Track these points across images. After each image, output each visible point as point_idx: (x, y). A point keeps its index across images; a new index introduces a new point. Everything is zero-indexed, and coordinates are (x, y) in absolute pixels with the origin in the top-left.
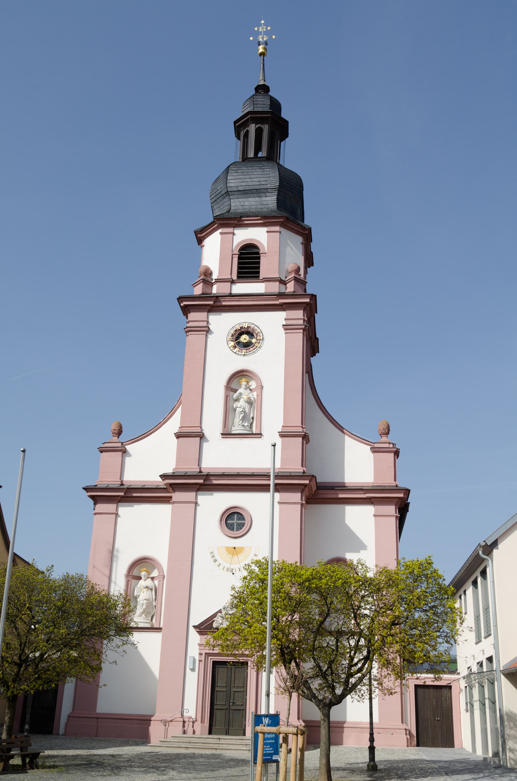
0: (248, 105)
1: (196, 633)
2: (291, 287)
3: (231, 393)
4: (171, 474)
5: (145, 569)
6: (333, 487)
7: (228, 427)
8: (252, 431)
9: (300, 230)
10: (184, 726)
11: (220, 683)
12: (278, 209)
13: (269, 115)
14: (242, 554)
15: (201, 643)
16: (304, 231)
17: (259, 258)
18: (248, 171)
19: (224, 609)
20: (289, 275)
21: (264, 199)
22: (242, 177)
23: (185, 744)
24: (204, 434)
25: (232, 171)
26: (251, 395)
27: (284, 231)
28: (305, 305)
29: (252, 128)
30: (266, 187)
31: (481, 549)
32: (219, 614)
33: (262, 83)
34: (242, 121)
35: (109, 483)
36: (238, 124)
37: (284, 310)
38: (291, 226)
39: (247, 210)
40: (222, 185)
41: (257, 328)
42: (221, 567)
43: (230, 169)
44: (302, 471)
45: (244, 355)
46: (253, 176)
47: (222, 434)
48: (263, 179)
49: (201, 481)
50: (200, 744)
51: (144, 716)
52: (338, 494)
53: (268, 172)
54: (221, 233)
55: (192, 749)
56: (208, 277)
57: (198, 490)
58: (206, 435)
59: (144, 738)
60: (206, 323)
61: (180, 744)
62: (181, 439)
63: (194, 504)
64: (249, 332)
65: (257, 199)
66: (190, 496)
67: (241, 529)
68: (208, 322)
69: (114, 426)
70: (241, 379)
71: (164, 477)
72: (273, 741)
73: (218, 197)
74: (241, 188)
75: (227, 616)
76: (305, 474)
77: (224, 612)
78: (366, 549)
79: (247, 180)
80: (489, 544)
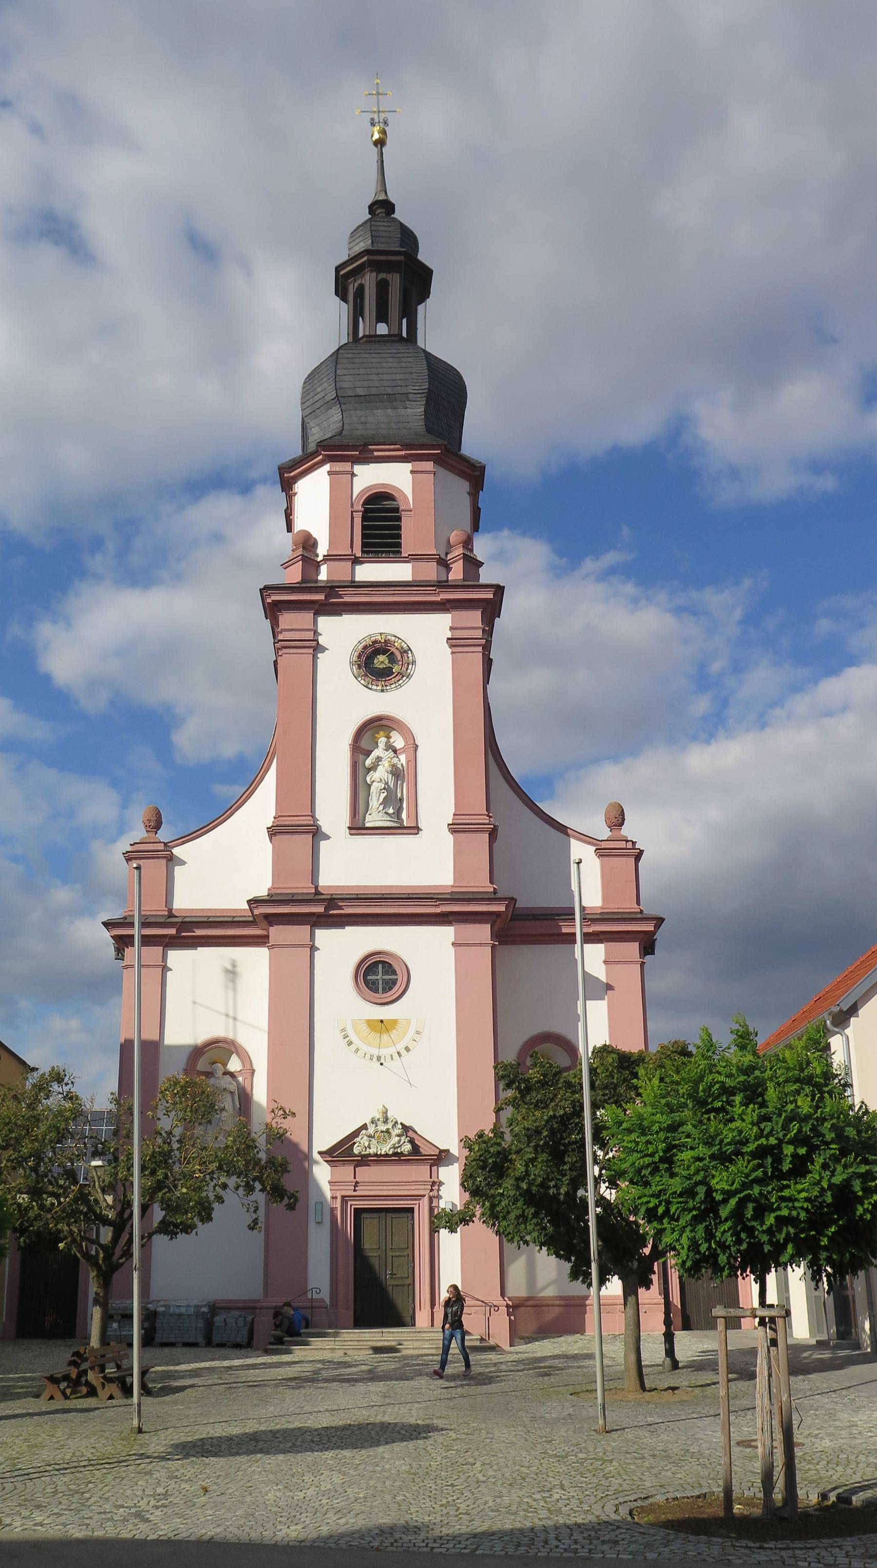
3: (361, 757)
4: (266, 898)
6: (534, 915)
9: (466, 469)
12: (429, 430)
13: (401, 258)
14: (394, 1031)
17: (399, 519)
18: (372, 360)
21: (402, 411)
22: (362, 371)
29: (369, 280)
30: (404, 390)
32: (364, 1132)
40: (326, 385)
43: (340, 356)
44: (492, 890)
45: (382, 691)
46: (382, 371)
47: (349, 828)
48: (398, 377)
50: (352, 1343)
54: (329, 473)
62: (279, 837)
63: (309, 949)
66: (301, 932)
67: (391, 989)
70: (378, 733)
71: (254, 902)
73: (318, 405)
74: (360, 392)
77: (371, 1130)
79: (371, 377)
80: (845, 1010)
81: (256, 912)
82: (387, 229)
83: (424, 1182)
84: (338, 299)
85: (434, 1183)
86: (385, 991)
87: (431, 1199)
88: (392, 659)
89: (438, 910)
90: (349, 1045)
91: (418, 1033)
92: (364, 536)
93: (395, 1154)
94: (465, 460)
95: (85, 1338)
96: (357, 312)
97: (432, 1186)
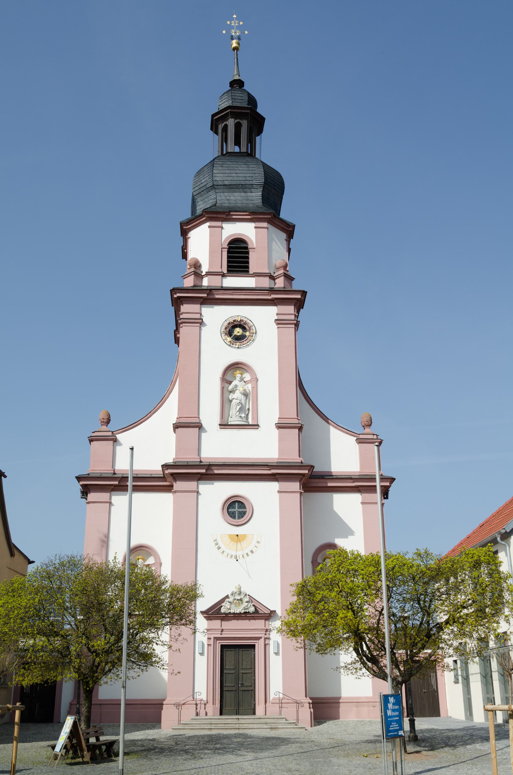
0: (226, 100)
1: (204, 618)
2: (280, 283)
3: (227, 385)
4: (172, 464)
5: (140, 557)
6: (322, 476)
8: (248, 422)
10: (197, 709)
11: (228, 665)
13: (249, 111)
14: (245, 542)
15: (209, 628)
16: (288, 228)
17: (248, 253)
18: (233, 166)
19: (232, 594)
20: (277, 271)
21: (249, 194)
22: (228, 171)
23: (207, 725)
25: (218, 165)
26: (245, 387)
27: (272, 228)
28: (296, 301)
29: (231, 123)
30: (251, 182)
31: (499, 536)
32: (227, 600)
33: (237, 78)
34: (220, 115)
35: (102, 472)
36: (216, 117)
38: (277, 222)
39: (233, 205)
40: (207, 178)
42: (225, 554)
43: (215, 163)
47: (220, 425)
48: (248, 175)
49: (204, 471)
50: (221, 725)
51: (147, 700)
52: (327, 483)
53: (254, 169)
54: (209, 227)
55: (215, 730)
56: (197, 269)
57: (199, 479)
58: (204, 425)
59: (155, 721)
61: (202, 725)
64: (241, 325)
65: (243, 194)
66: (191, 485)
67: (242, 517)
69: (102, 415)
70: (236, 371)
71: (165, 466)
72: (398, 718)
74: (226, 183)
75: (235, 601)
76: (303, 464)
78: (354, 535)
79: (232, 175)
80: (508, 531)
81: (167, 472)
82: (240, 95)
83: (261, 630)
84: (212, 132)
85: (267, 631)
86: (239, 518)
87: (265, 639)
88: (244, 329)
89: (270, 472)
90: (218, 549)
91: (258, 542)
92: (228, 262)
93: (245, 613)
94: (282, 221)
96: (225, 139)
97: (266, 632)
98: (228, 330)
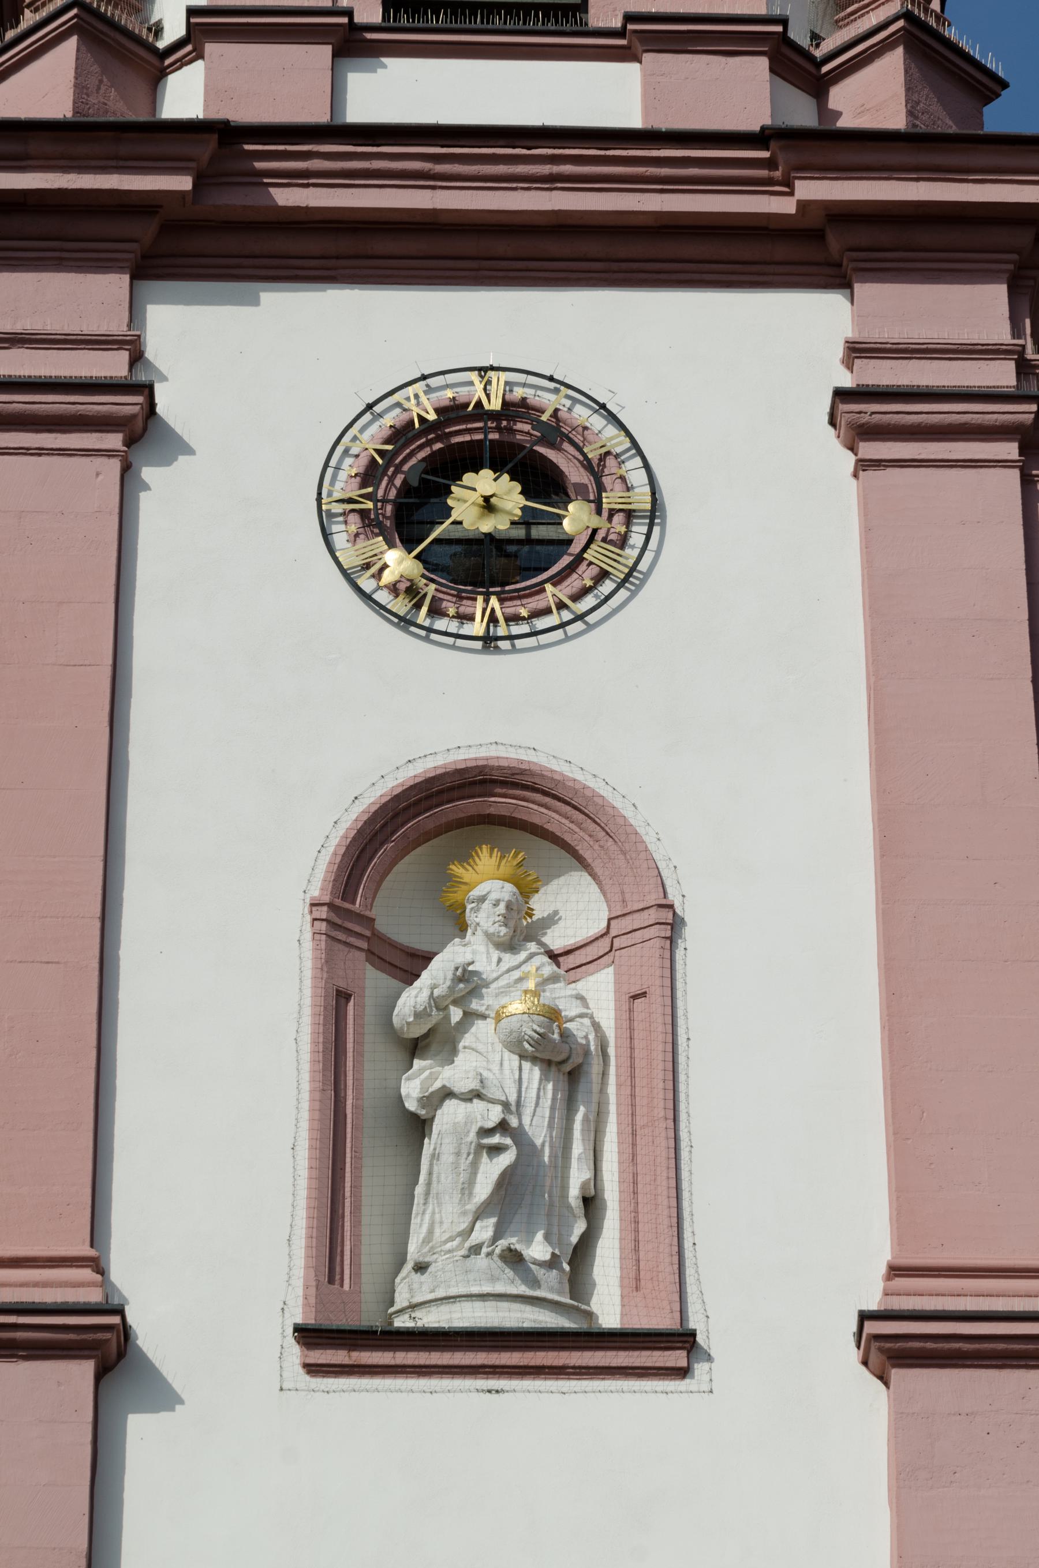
2: (875, 97)
3: (374, 980)
7: (356, 1275)
24: (125, 1332)
37: (835, 277)
41: (597, 422)
45: (489, 641)
60: (124, 356)
64: (517, 438)
68: (137, 357)
70: (465, 857)
88: (543, 483)
95: (184, 198)
98: (388, 488)
